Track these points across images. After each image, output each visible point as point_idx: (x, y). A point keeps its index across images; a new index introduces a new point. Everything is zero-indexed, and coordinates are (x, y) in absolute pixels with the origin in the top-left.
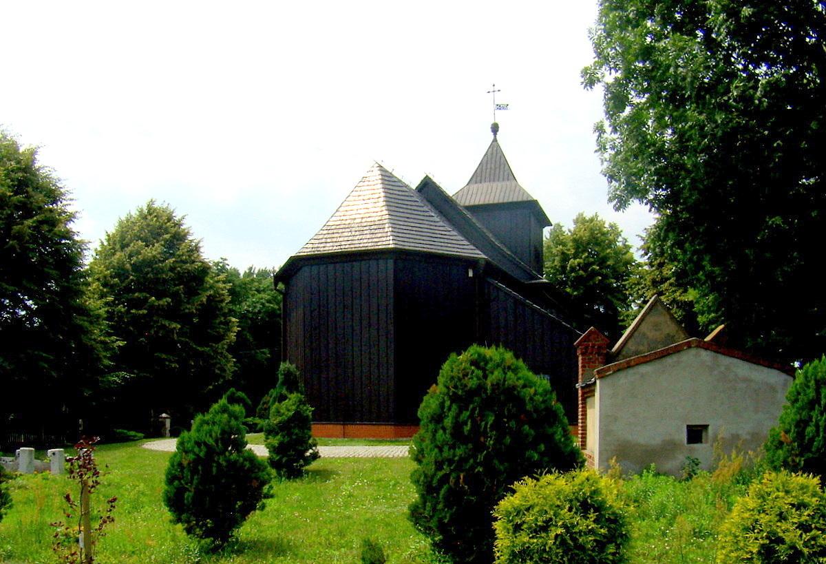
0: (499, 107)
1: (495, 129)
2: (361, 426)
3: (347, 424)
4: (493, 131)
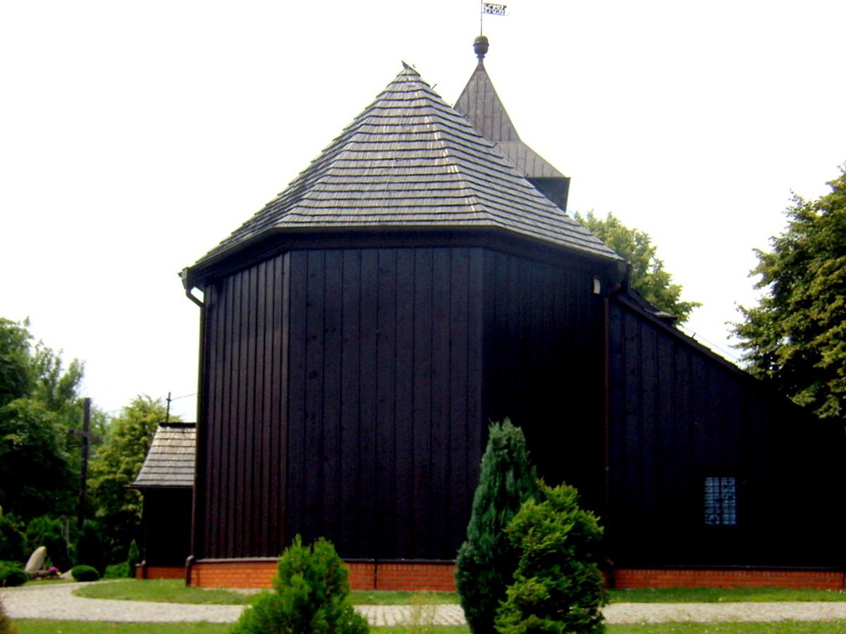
0: (490, 9)
1: (481, 47)
2: (410, 567)
3: (382, 563)
4: (477, 51)
